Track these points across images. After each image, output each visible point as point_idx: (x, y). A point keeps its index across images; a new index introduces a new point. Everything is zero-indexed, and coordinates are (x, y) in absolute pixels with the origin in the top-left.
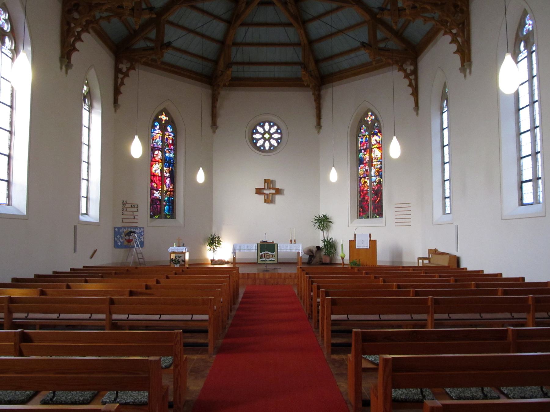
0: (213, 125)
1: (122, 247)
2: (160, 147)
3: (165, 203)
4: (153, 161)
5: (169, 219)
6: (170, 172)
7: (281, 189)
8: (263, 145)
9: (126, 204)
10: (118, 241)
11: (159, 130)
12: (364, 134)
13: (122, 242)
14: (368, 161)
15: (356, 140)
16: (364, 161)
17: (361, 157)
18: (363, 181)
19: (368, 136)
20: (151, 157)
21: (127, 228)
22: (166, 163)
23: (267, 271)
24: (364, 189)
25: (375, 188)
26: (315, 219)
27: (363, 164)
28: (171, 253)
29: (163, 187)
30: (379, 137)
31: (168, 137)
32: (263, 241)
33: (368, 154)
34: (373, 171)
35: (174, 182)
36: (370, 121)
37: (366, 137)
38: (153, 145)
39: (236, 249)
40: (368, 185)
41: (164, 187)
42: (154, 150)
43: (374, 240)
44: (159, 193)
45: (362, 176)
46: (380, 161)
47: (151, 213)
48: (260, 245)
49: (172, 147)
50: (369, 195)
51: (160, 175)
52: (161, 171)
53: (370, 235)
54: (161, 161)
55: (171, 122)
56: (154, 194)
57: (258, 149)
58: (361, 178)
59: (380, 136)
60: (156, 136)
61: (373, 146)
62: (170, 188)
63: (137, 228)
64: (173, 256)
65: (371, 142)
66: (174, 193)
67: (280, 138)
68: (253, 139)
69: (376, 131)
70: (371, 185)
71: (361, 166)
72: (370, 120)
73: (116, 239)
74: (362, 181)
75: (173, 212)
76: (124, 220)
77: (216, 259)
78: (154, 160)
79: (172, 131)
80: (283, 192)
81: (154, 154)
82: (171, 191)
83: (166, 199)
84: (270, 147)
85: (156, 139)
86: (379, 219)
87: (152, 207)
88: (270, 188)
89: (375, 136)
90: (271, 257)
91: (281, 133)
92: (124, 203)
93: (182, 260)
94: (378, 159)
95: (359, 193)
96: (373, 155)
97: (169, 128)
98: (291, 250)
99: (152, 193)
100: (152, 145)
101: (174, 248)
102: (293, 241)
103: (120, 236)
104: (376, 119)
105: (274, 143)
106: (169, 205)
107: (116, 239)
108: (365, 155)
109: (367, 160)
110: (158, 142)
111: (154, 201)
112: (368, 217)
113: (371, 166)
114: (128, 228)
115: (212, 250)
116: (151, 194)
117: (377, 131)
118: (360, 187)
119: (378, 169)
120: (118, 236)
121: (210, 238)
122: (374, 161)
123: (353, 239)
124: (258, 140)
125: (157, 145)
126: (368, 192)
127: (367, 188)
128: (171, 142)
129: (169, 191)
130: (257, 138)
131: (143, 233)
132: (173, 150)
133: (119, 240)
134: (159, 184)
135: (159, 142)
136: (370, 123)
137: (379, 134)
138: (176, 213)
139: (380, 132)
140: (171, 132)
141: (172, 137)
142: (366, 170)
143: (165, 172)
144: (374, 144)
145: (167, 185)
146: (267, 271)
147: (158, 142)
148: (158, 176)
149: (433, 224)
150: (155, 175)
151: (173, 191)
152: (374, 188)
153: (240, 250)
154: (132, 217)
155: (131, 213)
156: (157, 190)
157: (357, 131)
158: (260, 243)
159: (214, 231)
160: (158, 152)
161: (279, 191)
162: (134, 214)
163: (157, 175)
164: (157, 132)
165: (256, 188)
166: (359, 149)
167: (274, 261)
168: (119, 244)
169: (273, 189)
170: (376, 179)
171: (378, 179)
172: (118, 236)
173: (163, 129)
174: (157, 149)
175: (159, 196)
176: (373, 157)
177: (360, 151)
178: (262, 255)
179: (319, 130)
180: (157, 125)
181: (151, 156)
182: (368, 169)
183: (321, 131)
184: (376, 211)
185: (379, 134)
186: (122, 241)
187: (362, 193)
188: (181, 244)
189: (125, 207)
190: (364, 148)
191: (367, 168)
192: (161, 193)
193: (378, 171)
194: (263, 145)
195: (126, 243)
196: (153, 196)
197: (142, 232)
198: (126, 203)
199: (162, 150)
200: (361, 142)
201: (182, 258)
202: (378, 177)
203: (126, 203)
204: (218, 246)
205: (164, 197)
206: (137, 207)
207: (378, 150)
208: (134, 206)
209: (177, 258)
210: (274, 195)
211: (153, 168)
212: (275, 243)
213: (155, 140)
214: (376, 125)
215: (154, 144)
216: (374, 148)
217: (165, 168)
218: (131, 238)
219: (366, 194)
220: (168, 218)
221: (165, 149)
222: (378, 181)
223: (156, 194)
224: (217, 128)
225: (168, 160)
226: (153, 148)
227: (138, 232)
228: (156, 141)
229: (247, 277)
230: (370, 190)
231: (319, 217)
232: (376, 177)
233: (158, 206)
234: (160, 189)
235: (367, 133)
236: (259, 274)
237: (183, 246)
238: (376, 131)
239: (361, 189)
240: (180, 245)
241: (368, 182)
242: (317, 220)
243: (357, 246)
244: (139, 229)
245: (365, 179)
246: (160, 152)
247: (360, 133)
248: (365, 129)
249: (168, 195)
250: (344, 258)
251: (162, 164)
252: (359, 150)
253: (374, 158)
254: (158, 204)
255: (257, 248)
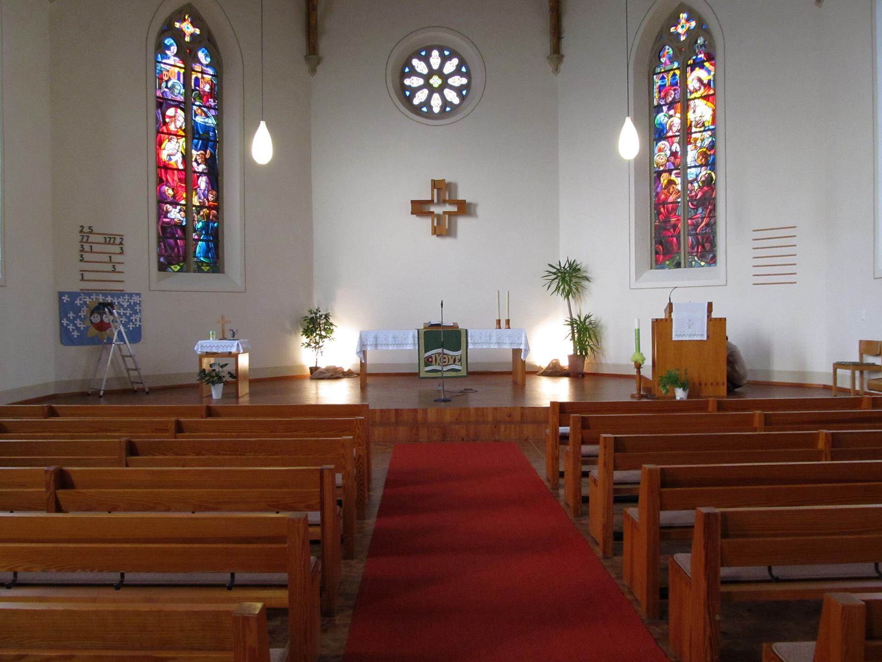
0: (310, 54)
1: (81, 341)
2: (181, 98)
3: (197, 235)
4: (163, 133)
5: (206, 272)
6: (206, 161)
7: (470, 204)
8: (427, 103)
9: (91, 236)
10: (71, 327)
11: (177, 59)
12: (668, 68)
13: (82, 329)
14: (678, 131)
15: (649, 83)
16: (667, 132)
17: (661, 124)
18: (666, 181)
19: (678, 72)
20: (157, 123)
21: (94, 294)
22: (196, 139)
23: (445, 401)
24: (667, 197)
25: (696, 195)
26: (550, 272)
27: (666, 138)
28: (201, 357)
29: (189, 198)
30: (709, 72)
31: (199, 75)
32: (432, 323)
33: (678, 115)
34: (692, 155)
35: (218, 187)
36: (683, 35)
37: (674, 75)
38: (162, 94)
39: (367, 344)
40: (677, 189)
41: (192, 197)
42: (164, 105)
43: (721, 319)
44: (180, 210)
45: (662, 168)
46: (709, 130)
47: (162, 259)
48: (425, 332)
49: (211, 102)
50: (680, 212)
51: (181, 167)
52: (183, 157)
53: (710, 305)
54: (183, 134)
55: (207, 40)
56: (167, 212)
57: (417, 110)
58: (659, 174)
59: (711, 68)
60: (168, 71)
61: (690, 95)
62: (208, 199)
63: (123, 295)
64: (206, 363)
65: (687, 86)
66: (218, 212)
67: (467, 87)
68: (404, 88)
69: (700, 56)
70: (685, 188)
71: (659, 144)
72: (683, 33)
73: (65, 322)
74: (662, 179)
75: (218, 257)
76: (87, 276)
77: (323, 365)
78: (165, 131)
79: (210, 62)
80: (475, 211)
81: (164, 116)
82: (209, 208)
83: (199, 225)
84: (443, 108)
85: (170, 79)
86: (707, 268)
87: (162, 244)
88: (445, 202)
89: (697, 69)
90: (451, 361)
91: (467, 75)
92: (86, 233)
93: (229, 373)
94: (703, 125)
95: (655, 209)
96: (691, 116)
97: (201, 55)
98: (499, 343)
99: (163, 210)
100: (159, 94)
101: (212, 344)
102: (503, 324)
103: (77, 315)
104: (702, 28)
105: (452, 96)
106: (207, 241)
107: (65, 322)
108: (671, 116)
109: (675, 129)
110: (173, 86)
111: (169, 230)
112: (678, 265)
113: (685, 142)
114: (97, 294)
115: (313, 345)
116: (161, 211)
117: (701, 56)
118: (657, 194)
119: (705, 150)
120: (71, 315)
121: (307, 317)
122: (694, 130)
123: (662, 315)
124: (414, 91)
125: (173, 93)
126: (677, 207)
127: (675, 196)
128: (207, 88)
129: (206, 207)
130: (413, 86)
131: (140, 306)
132: (214, 109)
133: (75, 325)
134: (180, 189)
135: (177, 87)
136: (683, 38)
137: (707, 64)
138: (223, 260)
139: (710, 58)
140: (207, 66)
141: (210, 77)
142: (674, 154)
143: (193, 159)
144: (695, 89)
145: (201, 192)
146: (445, 401)
147: (173, 86)
148: (178, 170)
149: (876, 277)
150: (170, 166)
151: (217, 206)
152: (693, 196)
153: (376, 345)
154: (109, 267)
155: (106, 258)
156: (175, 204)
157: (651, 61)
158: (425, 328)
159: (317, 302)
160: (176, 112)
161: (464, 209)
162: (113, 260)
163: (175, 166)
164: (171, 61)
165: (412, 202)
166: (655, 103)
167: (459, 370)
168: (75, 334)
169: (452, 202)
170: (700, 172)
171: (704, 172)
172: (71, 315)
173: (187, 55)
174: (172, 103)
175: (182, 219)
176: (692, 119)
177: (659, 109)
178: (430, 357)
179: (557, 66)
180: (171, 45)
181: (157, 119)
182: (678, 150)
183: (562, 67)
184: (698, 248)
185: (707, 64)
186: (82, 327)
187: (662, 210)
188: (228, 334)
189: (87, 242)
190: (668, 101)
191: (676, 147)
192: (185, 211)
193: (704, 155)
194: (427, 103)
195: (93, 332)
196: (166, 217)
197: (135, 304)
198: (91, 232)
199: (185, 106)
200: (660, 86)
201: (230, 368)
202: (703, 168)
203: (91, 232)
204: (325, 337)
205: (194, 220)
206: (121, 243)
207: (705, 102)
208: (112, 240)
209: (217, 368)
210: (453, 218)
211: (164, 149)
212: (460, 328)
213: (167, 82)
214: (699, 42)
215: (165, 92)
216: (695, 98)
217: (194, 152)
218: (106, 319)
219: (674, 209)
220: (206, 270)
221: (194, 104)
222: (703, 179)
223: (172, 213)
224: (319, 61)
225: (201, 133)
226: (161, 101)
227: (125, 304)
228: (170, 84)
229: (393, 420)
230: (684, 199)
231: (559, 268)
232: (699, 168)
233: (178, 241)
234: (183, 202)
235: (676, 65)
236: (425, 411)
237: (234, 336)
238: (700, 56)
239: (659, 199)
240: (225, 337)
241: (678, 181)
242: (554, 274)
243: (676, 335)
244: (126, 297)
245: (670, 174)
246: (181, 113)
247: (658, 66)
248: (671, 56)
249: (203, 215)
250: (640, 365)
251: (186, 141)
252: (655, 107)
253: (693, 124)
254: (179, 238)
255: (417, 340)
